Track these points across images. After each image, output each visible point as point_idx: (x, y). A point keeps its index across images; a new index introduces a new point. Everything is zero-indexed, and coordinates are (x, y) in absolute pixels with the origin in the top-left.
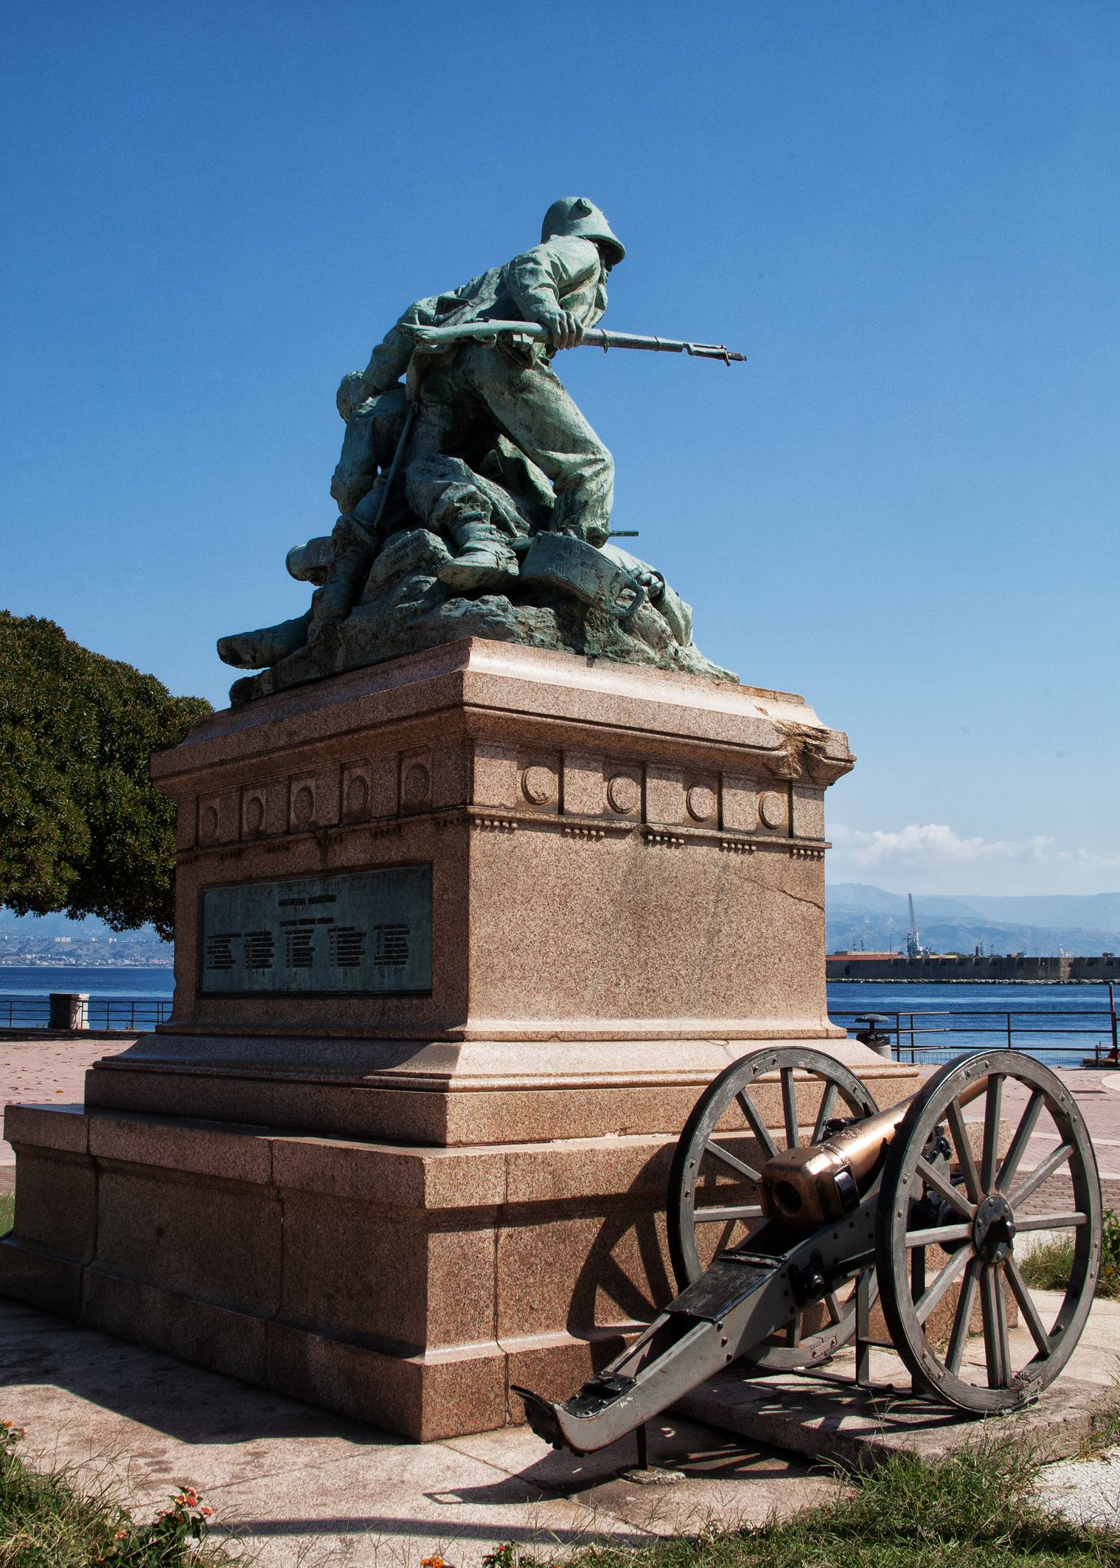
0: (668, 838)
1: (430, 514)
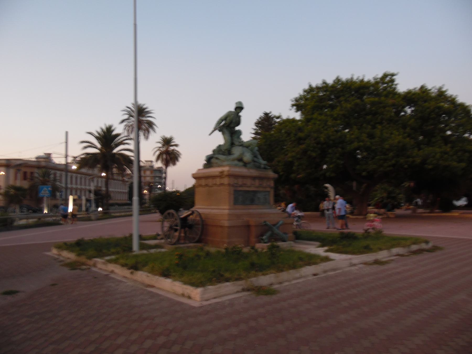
0: (212, 187)
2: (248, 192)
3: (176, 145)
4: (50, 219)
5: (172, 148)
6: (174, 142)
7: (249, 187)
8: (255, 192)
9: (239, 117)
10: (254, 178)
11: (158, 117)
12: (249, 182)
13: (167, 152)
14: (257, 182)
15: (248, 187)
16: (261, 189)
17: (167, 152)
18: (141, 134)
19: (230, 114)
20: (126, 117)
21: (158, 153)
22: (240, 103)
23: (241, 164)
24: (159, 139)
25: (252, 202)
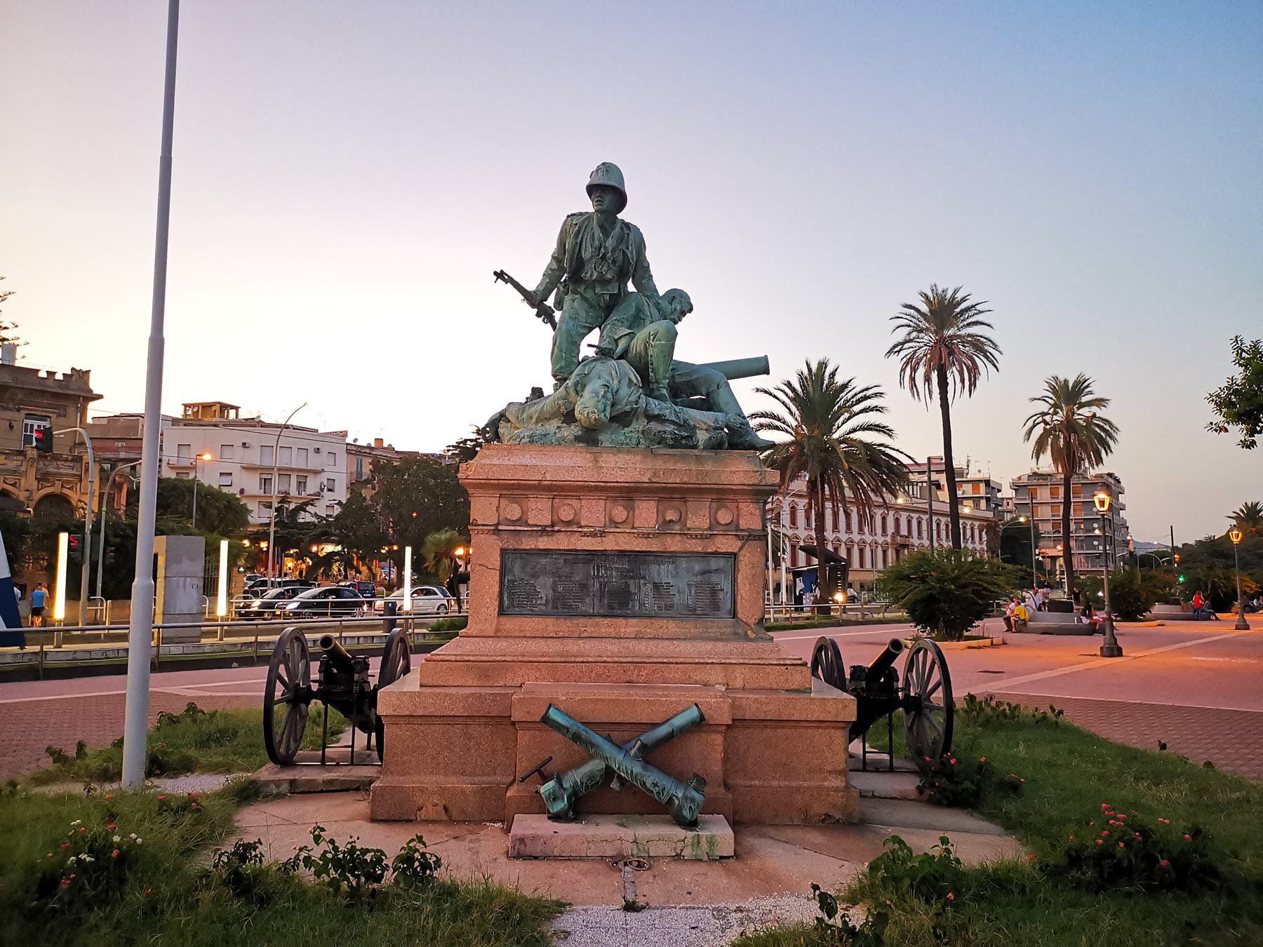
1: (1089, 404)
2: (592, 556)
3: (1100, 402)
4: (851, 615)
5: (1086, 412)
6: (1091, 393)
7: (603, 534)
8: (636, 559)
9: (631, 240)
10: (628, 494)
11: (999, 325)
12: (593, 512)
13: (1070, 426)
14: (647, 513)
15: (593, 535)
16: (674, 544)
17: (1070, 426)
18: (953, 376)
19: (575, 228)
20: (902, 334)
21: (1039, 430)
22: (607, 168)
23: (570, 431)
24: (1042, 390)
25: (619, 603)
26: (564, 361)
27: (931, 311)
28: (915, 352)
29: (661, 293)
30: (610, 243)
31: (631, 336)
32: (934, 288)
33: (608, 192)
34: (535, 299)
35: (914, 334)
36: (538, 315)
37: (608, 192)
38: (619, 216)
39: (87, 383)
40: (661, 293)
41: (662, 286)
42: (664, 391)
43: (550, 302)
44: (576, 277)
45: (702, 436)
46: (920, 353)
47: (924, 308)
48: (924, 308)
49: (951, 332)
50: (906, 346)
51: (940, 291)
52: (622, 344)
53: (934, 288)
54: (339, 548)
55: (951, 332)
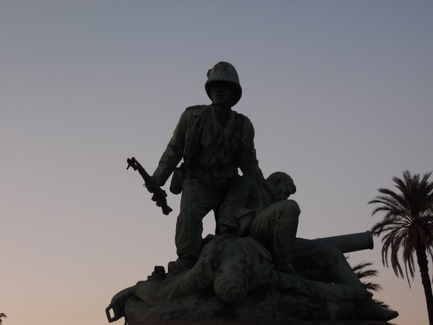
9: (243, 129)
19: (193, 117)
20: (381, 216)
26: (187, 230)
27: (405, 194)
28: (394, 233)
29: (266, 176)
30: (227, 132)
31: (253, 215)
32: (406, 175)
33: (224, 85)
34: (153, 184)
35: (392, 217)
36: (154, 199)
37: (224, 85)
38: (233, 108)
39: (428, 273)
40: (266, 176)
41: (267, 168)
42: (290, 266)
43: (166, 187)
44: (193, 164)
45: (333, 308)
46: (399, 233)
47: (399, 192)
48: (399, 192)
49: (425, 214)
50: (386, 227)
51: (412, 176)
52: (244, 223)
53: (406, 175)
54: (173, 173)
55: (425, 214)
